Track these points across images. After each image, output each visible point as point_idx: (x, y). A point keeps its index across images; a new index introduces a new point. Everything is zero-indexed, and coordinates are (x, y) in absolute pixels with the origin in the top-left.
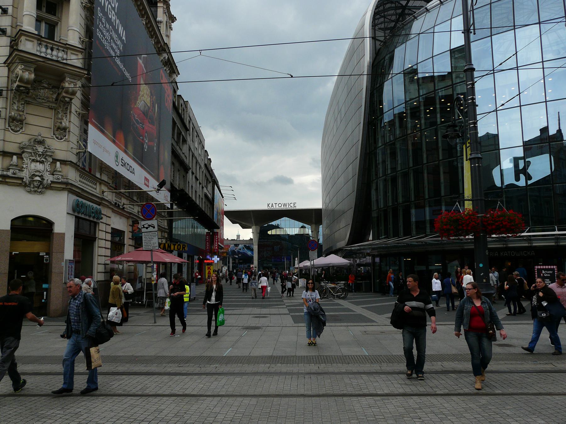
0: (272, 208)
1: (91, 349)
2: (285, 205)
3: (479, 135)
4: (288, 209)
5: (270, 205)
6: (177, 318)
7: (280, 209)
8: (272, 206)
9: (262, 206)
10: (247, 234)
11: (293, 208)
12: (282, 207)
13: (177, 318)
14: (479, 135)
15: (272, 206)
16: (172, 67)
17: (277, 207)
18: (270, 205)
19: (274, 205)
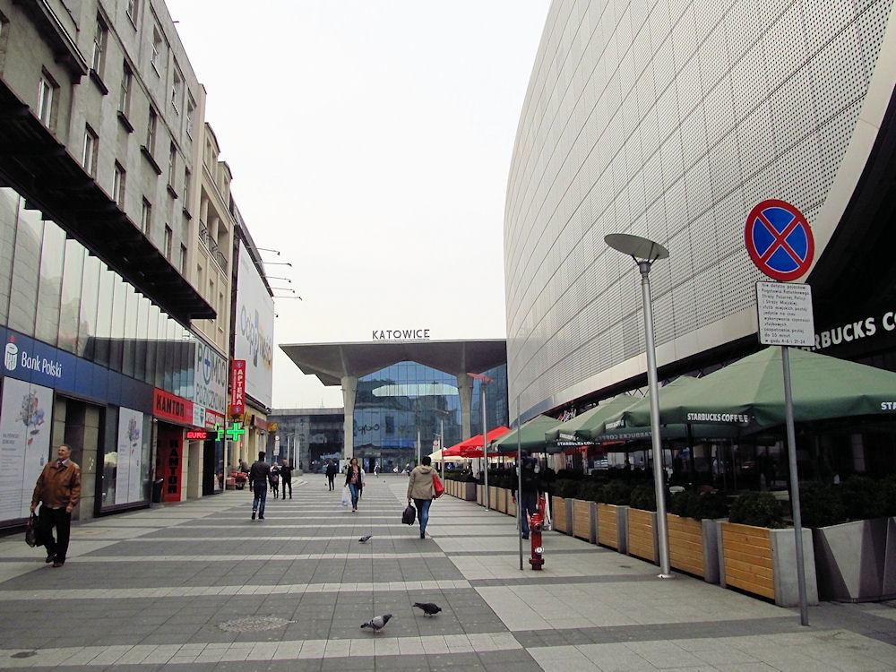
0: (382, 341)
1: (43, 546)
2: (407, 333)
3: (25, 534)
4: (414, 341)
5: (378, 335)
6: (287, 485)
7: (398, 341)
8: (382, 336)
9: (358, 333)
10: (333, 398)
11: (423, 340)
12: (412, 337)
13: (287, 485)
14: (25, 534)
15: (382, 336)
16: (759, 411)
17: (392, 338)
18: (378, 335)
19: (386, 335)
